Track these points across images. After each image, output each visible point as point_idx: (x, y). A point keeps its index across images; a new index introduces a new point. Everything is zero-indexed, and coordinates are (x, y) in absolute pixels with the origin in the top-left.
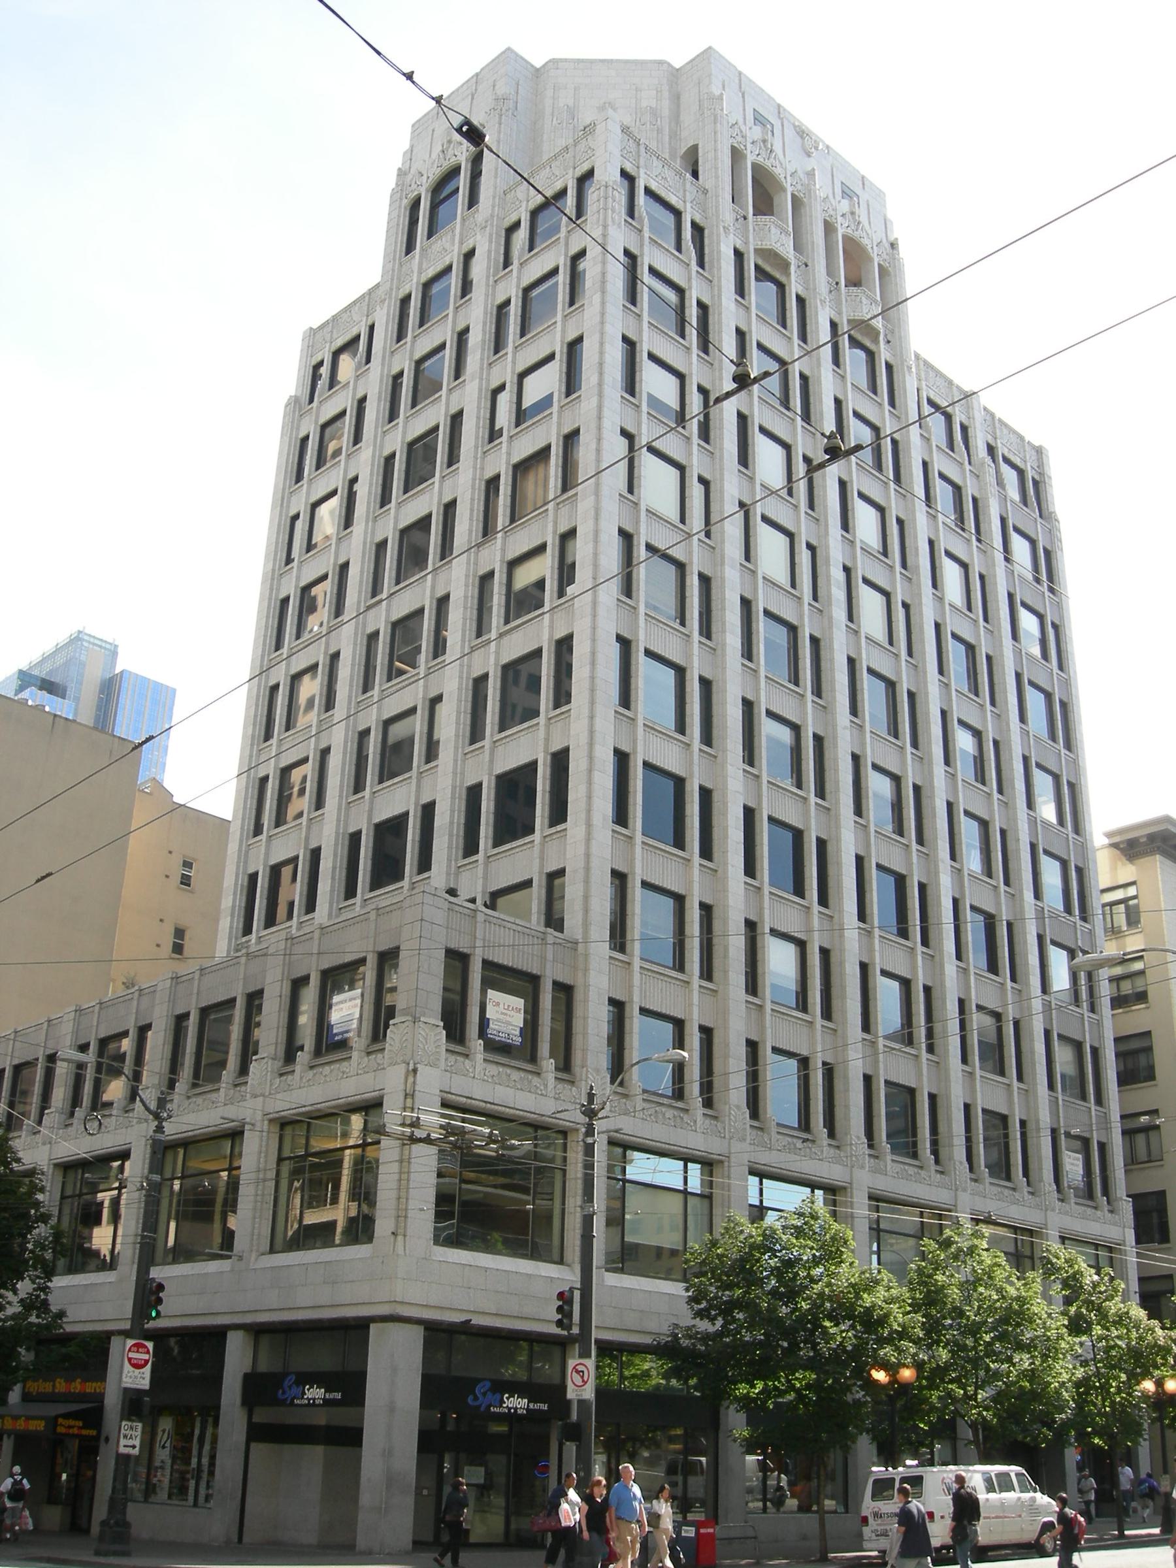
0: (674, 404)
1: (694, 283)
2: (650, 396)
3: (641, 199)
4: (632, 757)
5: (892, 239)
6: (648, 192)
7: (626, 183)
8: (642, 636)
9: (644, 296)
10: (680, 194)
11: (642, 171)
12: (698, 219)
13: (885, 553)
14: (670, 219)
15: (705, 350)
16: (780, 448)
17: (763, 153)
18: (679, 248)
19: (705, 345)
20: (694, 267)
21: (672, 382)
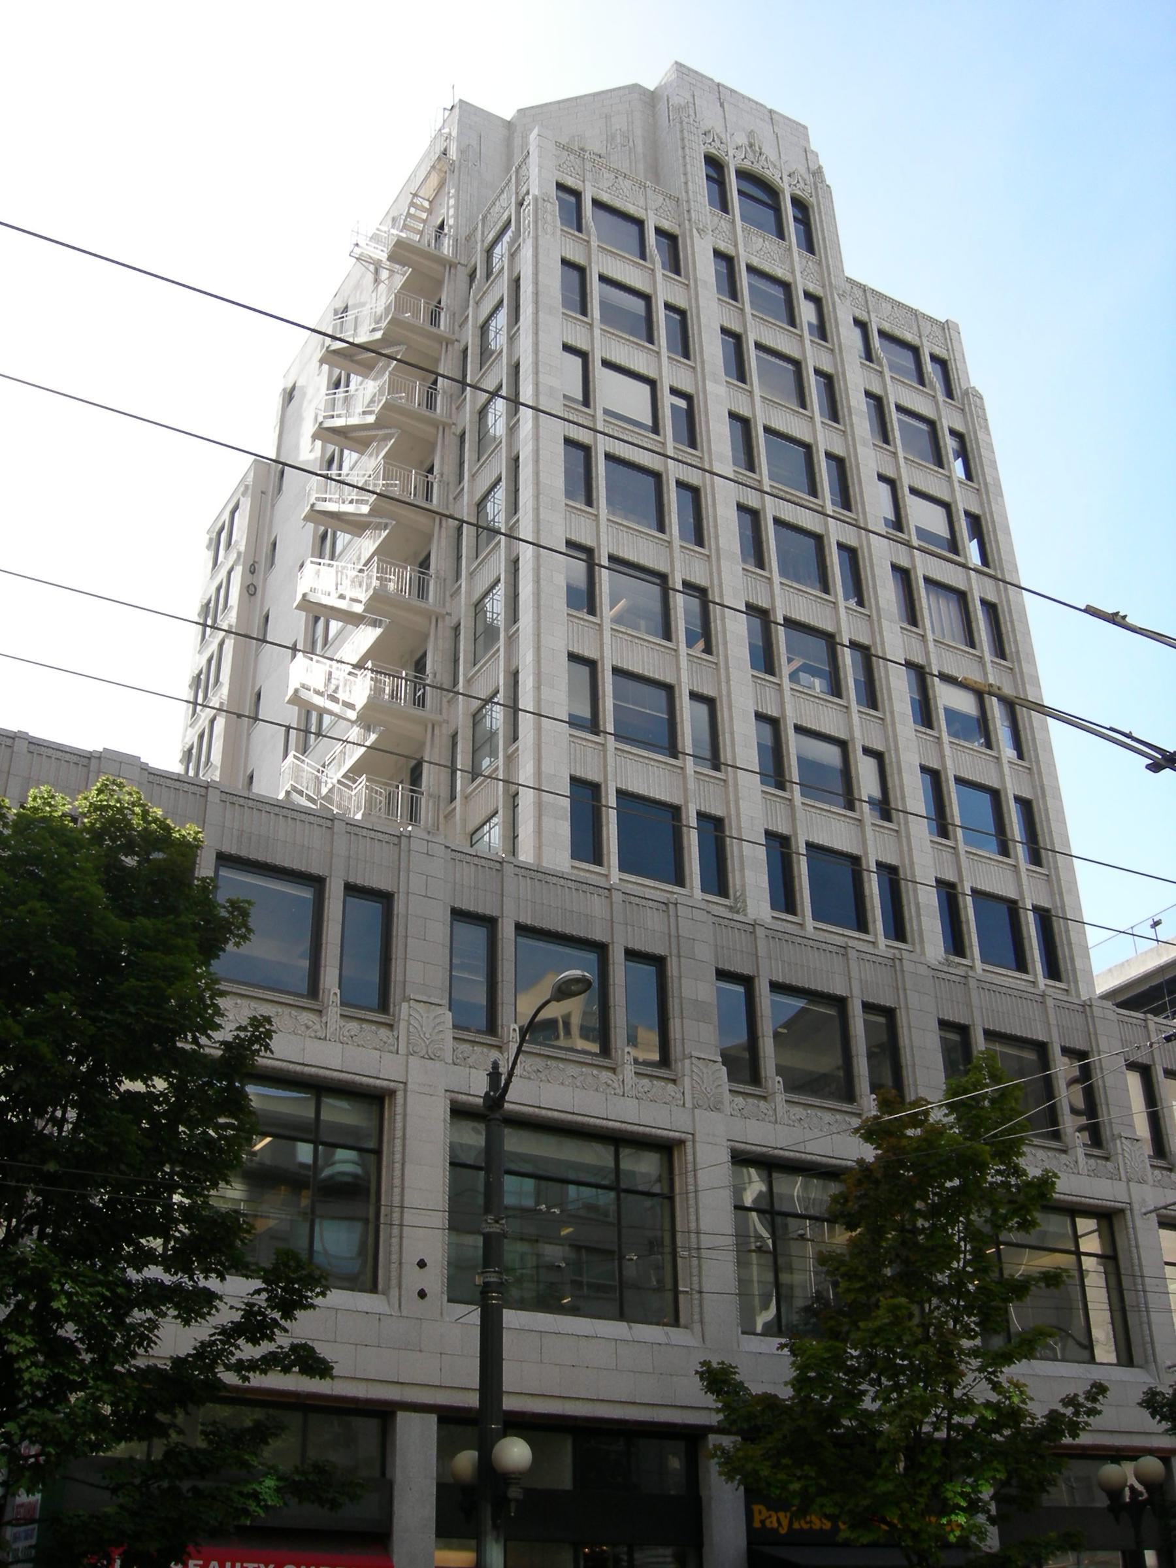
0: (944, 532)
1: (943, 413)
2: (918, 529)
3: (876, 341)
4: (726, 821)
5: (813, 167)
6: (882, 334)
7: (938, 367)
8: (857, 734)
9: (896, 434)
10: (642, 203)
11: (873, 315)
12: (666, 225)
13: (656, 429)
14: (778, 293)
15: (835, 417)
16: (939, 508)
17: (750, 155)
18: (922, 382)
19: (834, 412)
20: (941, 397)
21: (940, 512)
